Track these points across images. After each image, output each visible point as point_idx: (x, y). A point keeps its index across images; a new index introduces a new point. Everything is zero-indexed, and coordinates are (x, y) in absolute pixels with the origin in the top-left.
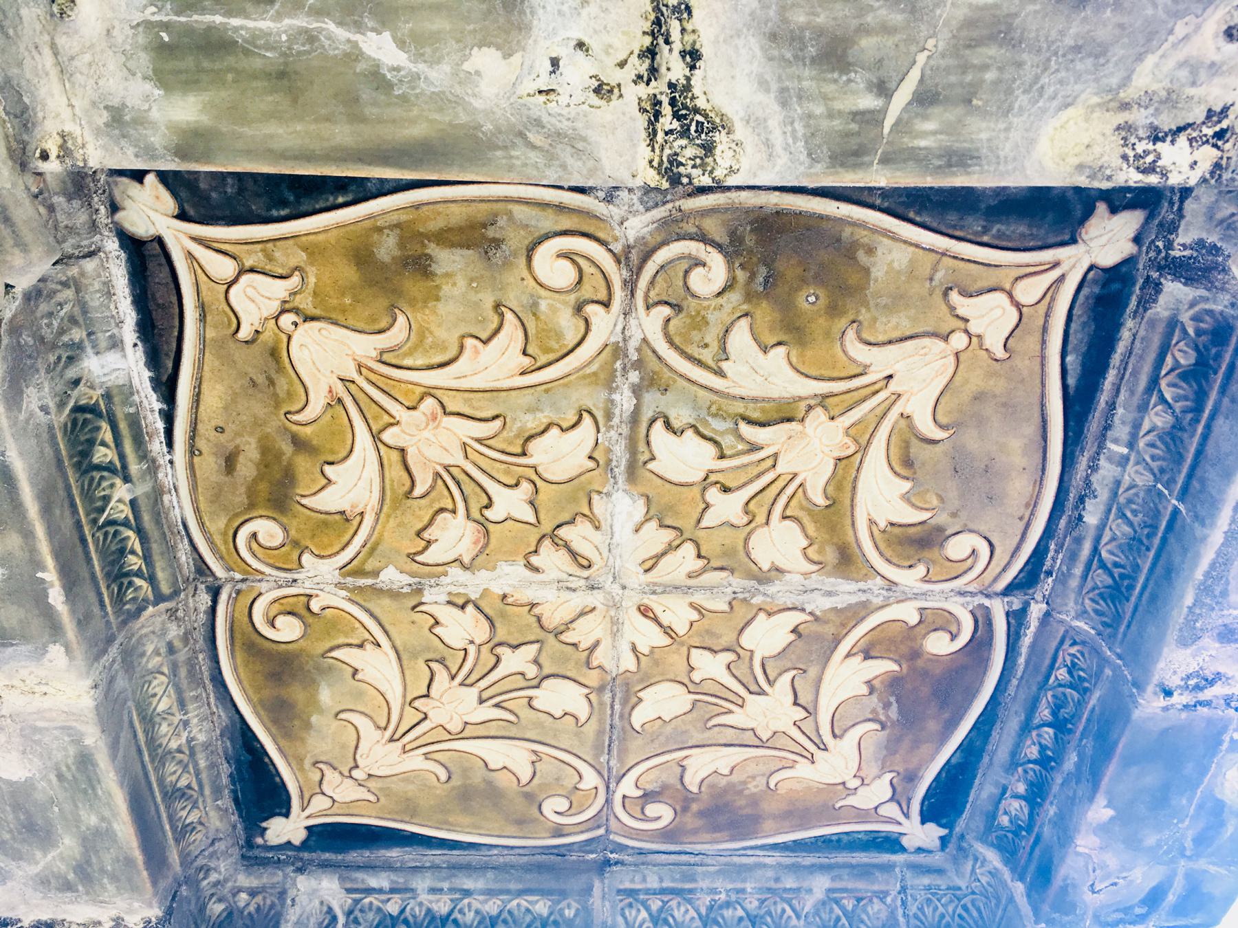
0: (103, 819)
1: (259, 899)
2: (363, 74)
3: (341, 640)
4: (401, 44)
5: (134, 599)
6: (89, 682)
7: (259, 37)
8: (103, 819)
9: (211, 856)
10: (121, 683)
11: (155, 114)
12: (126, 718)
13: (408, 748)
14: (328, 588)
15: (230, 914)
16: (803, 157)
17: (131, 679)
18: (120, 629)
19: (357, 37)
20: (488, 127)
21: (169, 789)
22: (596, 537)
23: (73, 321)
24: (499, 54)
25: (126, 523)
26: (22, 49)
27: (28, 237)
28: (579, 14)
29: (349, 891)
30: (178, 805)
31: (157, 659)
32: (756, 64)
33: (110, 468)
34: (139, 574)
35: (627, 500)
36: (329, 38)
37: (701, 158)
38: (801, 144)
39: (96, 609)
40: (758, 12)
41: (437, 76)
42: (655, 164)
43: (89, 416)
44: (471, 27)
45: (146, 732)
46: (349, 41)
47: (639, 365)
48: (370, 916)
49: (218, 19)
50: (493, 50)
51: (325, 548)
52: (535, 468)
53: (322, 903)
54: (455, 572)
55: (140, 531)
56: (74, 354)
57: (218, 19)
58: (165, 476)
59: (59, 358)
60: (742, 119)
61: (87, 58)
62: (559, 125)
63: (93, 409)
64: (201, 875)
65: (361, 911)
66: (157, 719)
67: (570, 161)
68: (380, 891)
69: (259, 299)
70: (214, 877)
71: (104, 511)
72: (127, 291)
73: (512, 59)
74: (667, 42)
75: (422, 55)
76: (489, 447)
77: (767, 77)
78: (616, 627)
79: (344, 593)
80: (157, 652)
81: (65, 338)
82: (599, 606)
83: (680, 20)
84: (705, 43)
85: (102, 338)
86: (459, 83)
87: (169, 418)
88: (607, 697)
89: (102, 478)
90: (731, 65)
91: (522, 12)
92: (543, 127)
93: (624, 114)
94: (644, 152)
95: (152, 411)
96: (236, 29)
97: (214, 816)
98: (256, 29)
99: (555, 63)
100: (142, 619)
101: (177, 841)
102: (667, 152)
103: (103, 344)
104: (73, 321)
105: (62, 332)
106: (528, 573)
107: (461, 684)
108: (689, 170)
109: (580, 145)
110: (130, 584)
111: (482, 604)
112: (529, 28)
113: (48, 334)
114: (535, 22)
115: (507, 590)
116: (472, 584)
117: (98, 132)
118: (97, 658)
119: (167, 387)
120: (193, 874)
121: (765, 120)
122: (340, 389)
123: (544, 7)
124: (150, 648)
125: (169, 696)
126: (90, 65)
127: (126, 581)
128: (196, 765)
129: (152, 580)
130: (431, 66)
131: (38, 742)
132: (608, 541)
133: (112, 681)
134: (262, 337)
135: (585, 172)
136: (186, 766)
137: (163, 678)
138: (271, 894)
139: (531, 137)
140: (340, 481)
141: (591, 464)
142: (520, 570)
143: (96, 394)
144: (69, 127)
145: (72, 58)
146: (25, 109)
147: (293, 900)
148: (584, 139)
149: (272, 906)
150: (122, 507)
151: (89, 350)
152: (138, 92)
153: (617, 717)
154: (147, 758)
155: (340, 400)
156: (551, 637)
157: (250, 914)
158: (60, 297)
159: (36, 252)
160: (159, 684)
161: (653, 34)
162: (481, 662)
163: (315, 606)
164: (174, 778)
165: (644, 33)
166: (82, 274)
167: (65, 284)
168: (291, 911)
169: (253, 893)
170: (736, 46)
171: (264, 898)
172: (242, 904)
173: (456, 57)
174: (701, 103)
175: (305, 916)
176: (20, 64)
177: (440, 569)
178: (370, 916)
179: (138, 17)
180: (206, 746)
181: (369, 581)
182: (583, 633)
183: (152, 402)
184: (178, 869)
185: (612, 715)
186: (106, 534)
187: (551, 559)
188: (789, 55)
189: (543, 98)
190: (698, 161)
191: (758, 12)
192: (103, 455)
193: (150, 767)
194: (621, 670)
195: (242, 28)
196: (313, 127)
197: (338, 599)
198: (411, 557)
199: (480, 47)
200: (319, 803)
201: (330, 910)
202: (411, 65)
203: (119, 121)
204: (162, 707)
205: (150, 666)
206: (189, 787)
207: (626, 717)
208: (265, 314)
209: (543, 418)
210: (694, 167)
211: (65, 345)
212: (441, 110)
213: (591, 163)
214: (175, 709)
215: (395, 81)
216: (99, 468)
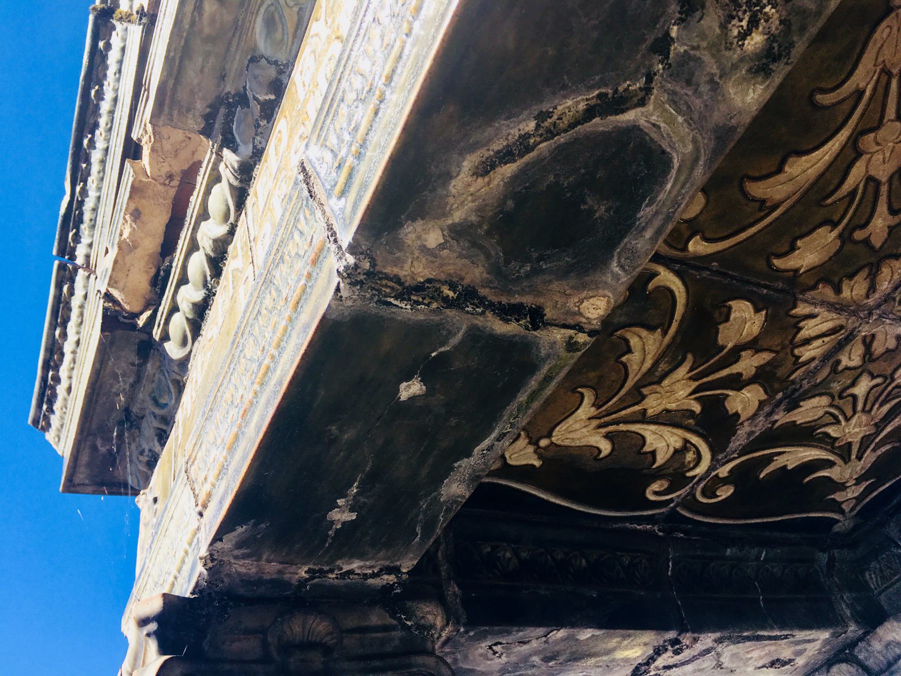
156: (873, 260)
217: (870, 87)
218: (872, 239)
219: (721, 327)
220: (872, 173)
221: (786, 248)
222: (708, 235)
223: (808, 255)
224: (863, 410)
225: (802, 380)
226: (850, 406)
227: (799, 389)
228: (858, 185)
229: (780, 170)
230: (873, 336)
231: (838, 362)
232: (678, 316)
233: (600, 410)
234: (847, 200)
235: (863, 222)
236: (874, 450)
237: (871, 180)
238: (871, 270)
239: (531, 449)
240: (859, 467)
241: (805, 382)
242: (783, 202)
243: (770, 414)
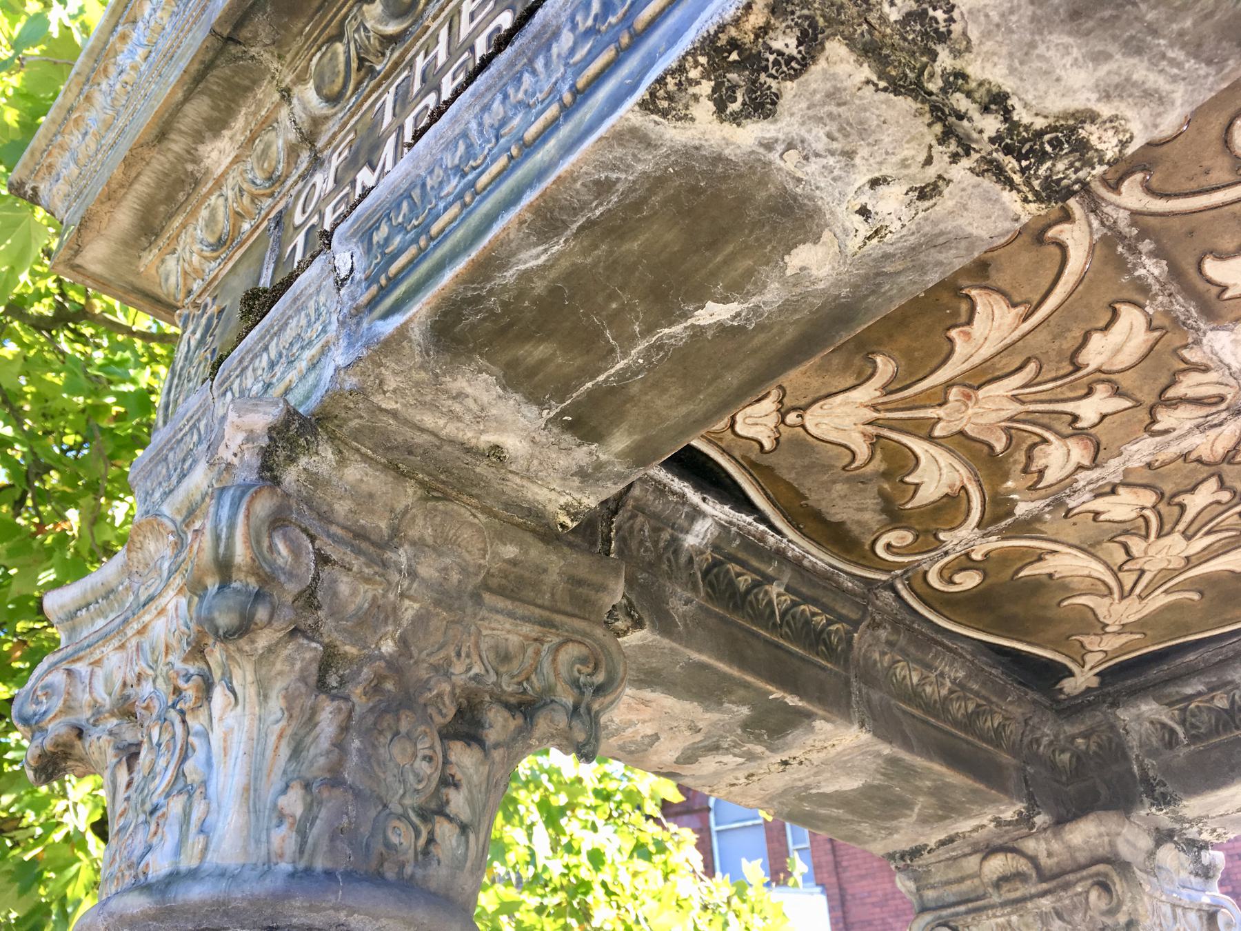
0: (934, 780)
1: (1094, 738)
2: (714, 336)
3: (1020, 565)
4: (725, 300)
5: (840, 639)
6: (856, 726)
7: (626, 373)
8: (934, 780)
9: (1032, 731)
10: (876, 696)
11: (603, 457)
12: (899, 714)
13: (1143, 595)
14: (978, 542)
15: (1079, 758)
16: (1203, 69)
17: (881, 689)
18: (847, 669)
19: (690, 322)
20: (845, 291)
21: (965, 720)
22: (1212, 376)
23: (656, 530)
24: (809, 245)
25: (795, 604)
26: (496, 485)
27: (597, 578)
28: (853, 166)
29: (1170, 704)
30: (979, 723)
31: (887, 658)
32: (1075, 50)
33: (756, 585)
34: (830, 623)
35: (1222, 334)
36: (672, 337)
37: (1079, 160)
38: (1191, 64)
39: (822, 675)
40: (1039, 12)
41: (772, 295)
42: (1030, 197)
43: (715, 570)
44: (769, 247)
45: (919, 706)
46: (686, 328)
47: (1144, 234)
48: (1205, 717)
49: (589, 385)
50: (801, 246)
51: (952, 522)
52: (1099, 370)
53: (1152, 723)
55: (807, 600)
56: (675, 545)
57: (589, 385)
58: (794, 551)
59: (669, 560)
60: (1099, 100)
61: (536, 462)
62: (907, 244)
63: (716, 564)
64: (1035, 747)
65: (1193, 715)
66: (920, 689)
67: (941, 257)
68: (1200, 694)
69: (759, 421)
70: (1045, 741)
71: (774, 612)
72: (670, 476)
73: (822, 239)
74: (960, 117)
75: (748, 292)
76: (1039, 384)
77: (1099, 47)
79: (995, 538)
80: (883, 654)
81: (662, 544)
83: (959, 90)
84: (1000, 81)
85: (682, 521)
86: (794, 285)
87: (763, 519)
89: (756, 596)
90: (1047, 73)
91: (801, 206)
92: (894, 255)
93: (963, 190)
94: (1010, 199)
95: (750, 524)
96: (606, 381)
97: (1012, 710)
98: (617, 371)
99: (864, 212)
100: (855, 645)
101: (998, 746)
102: (1036, 184)
103: (686, 524)
104: (656, 530)
105: (656, 543)
107: (1159, 536)
108: (1074, 177)
109: (941, 240)
110: (829, 634)
111: (1131, 480)
112: (817, 211)
113: (649, 556)
114: (820, 203)
115: (1148, 459)
117: (580, 490)
118: (849, 705)
119: (742, 502)
120: (1027, 752)
121: (1128, 80)
122: (871, 430)
123: (817, 188)
124: (877, 656)
125: (915, 670)
126: (541, 464)
127: (825, 636)
128: (971, 691)
129: (841, 618)
130: (761, 293)
131: (853, 766)
132: (1227, 373)
133: (869, 701)
134: (782, 439)
135: (963, 252)
136: (965, 697)
137: (901, 664)
138: (1103, 732)
139: (888, 269)
140: (925, 479)
141: (1157, 334)
143: (708, 554)
144: (562, 501)
145: (528, 470)
146: (529, 510)
147: (1124, 729)
148: (941, 233)
149: (1110, 740)
150: (783, 598)
151: (681, 536)
152: (582, 454)
154: (933, 720)
155: (878, 437)
156: (1225, 466)
157: (1095, 752)
158: (637, 526)
159: (611, 584)
160: (901, 670)
161: (939, 119)
163: (977, 556)
164: (962, 711)
165: (930, 125)
166: (636, 500)
167: (633, 517)
168: (1129, 738)
169: (1086, 736)
170: (1040, 57)
171: (1099, 736)
172: (1083, 747)
173: (777, 273)
174: (1040, 123)
175: (1144, 737)
176: (504, 493)
178: (1205, 717)
179: (542, 423)
180: (968, 676)
181: (1010, 520)
183: (745, 519)
184: (1014, 761)
186: (788, 623)
188: (1107, 13)
189: (875, 241)
190: (1077, 164)
191: (1039, 12)
192: (744, 582)
193: (940, 724)
195: (608, 377)
196: (710, 390)
197: (994, 543)
198: (1032, 488)
199: (789, 254)
200: (1091, 659)
201: (1164, 725)
202: (746, 305)
203: (586, 476)
204: (915, 680)
205: (886, 665)
206: (978, 706)
208: (772, 426)
209: (1077, 333)
210: (1076, 171)
211: (666, 548)
212: (795, 311)
213: (963, 244)
214: (926, 673)
215: (742, 322)
216: (748, 591)
217: (1157, 593)
218: (1215, 487)
220: (1184, 543)
224: (1139, 596)
233: (886, 399)
237: (1187, 536)
238: (1233, 457)
239: (772, 420)
240: (1132, 611)
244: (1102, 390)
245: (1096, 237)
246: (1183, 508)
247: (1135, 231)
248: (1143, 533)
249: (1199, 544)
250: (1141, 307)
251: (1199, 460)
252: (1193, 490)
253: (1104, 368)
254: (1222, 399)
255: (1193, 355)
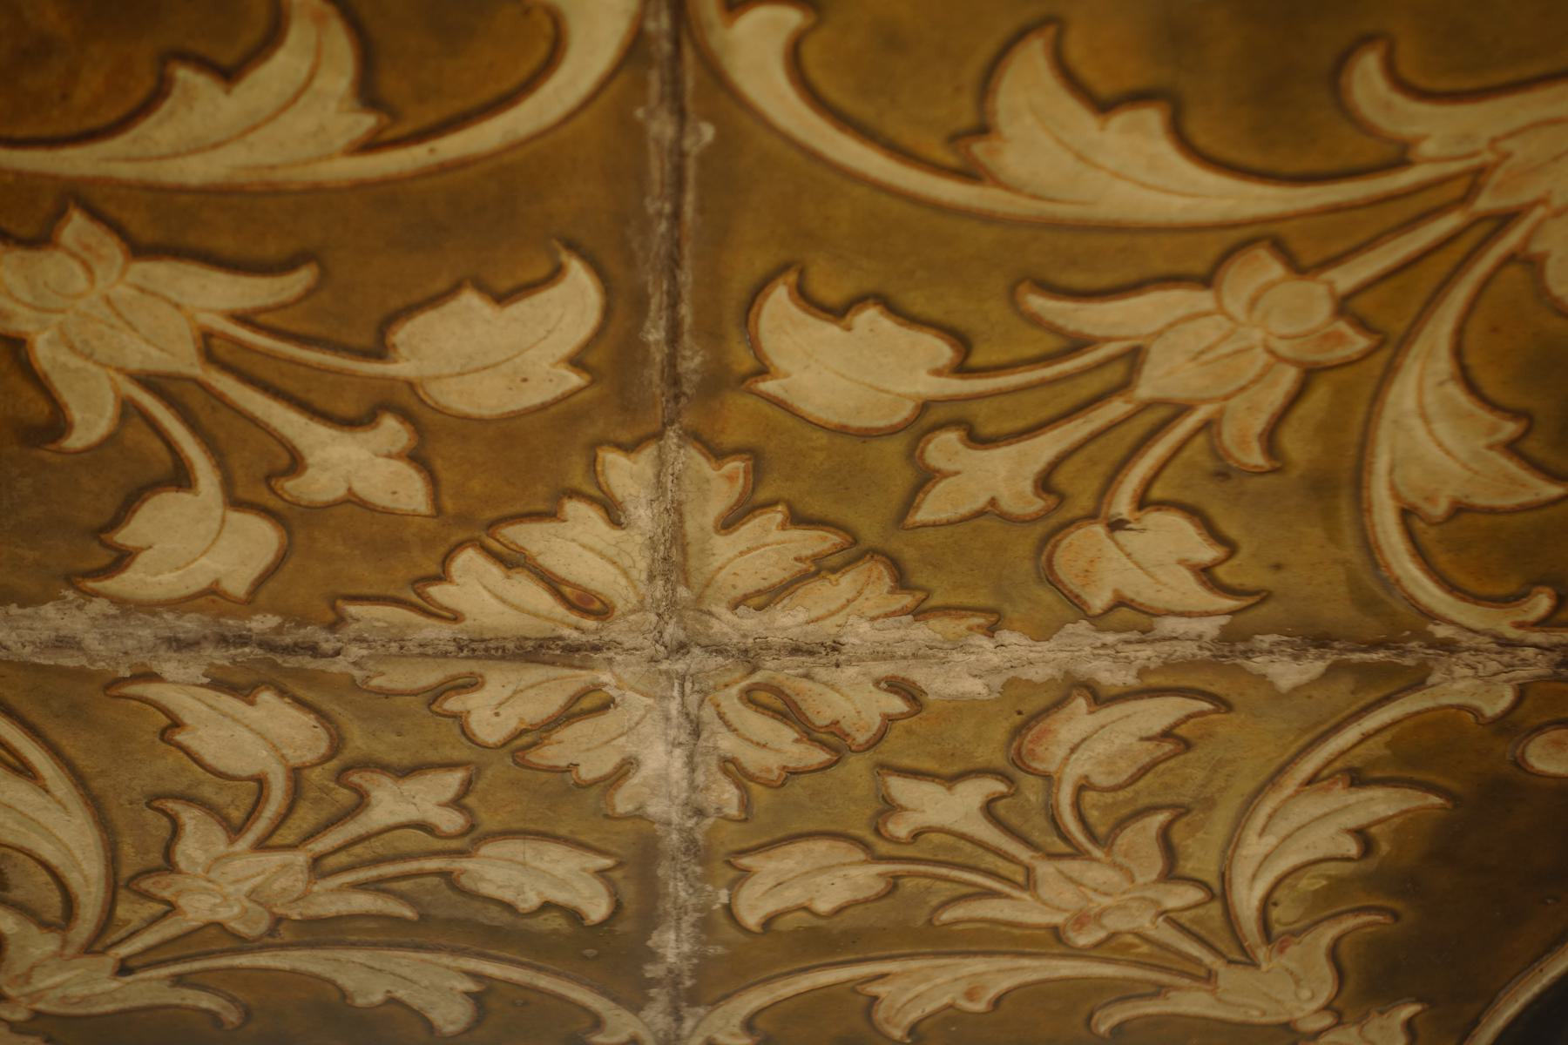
22: (727, 744)
54: (1111, 676)
78: (673, 557)
82: (721, 610)
88: (693, 361)
106: (918, 675)
107: (262, 846)
116: (1081, 651)
142: (939, 683)
153: (657, 301)
162: (1103, 468)
177: (1154, 681)
182: (769, 547)
185: (674, 301)
187: (852, 700)
194: (650, 452)
207: (623, 305)
219: (470, 300)
221: (832, 294)
222: (812, 54)
223: (839, 367)
225: (360, 640)
226: (326, 812)
227: (325, 655)
228: (1108, 340)
229: (1104, 107)
230: (606, 705)
231: (472, 684)
232: (452, 146)
234: (1050, 343)
235: (989, 429)
236: (179, 981)
241: (356, 651)
242: (1007, 187)
243: (179, 644)
244: (392, 431)
245: (701, 1011)
246: (362, 801)
247: (653, 992)
248: (237, 815)
249: (331, 901)
250: (729, 909)
251: (901, 581)
252: (404, 772)
253: (862, 856)
254: (749, 697)
255: (727, 796)
